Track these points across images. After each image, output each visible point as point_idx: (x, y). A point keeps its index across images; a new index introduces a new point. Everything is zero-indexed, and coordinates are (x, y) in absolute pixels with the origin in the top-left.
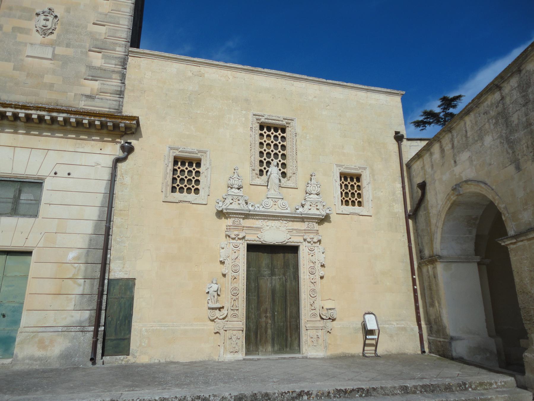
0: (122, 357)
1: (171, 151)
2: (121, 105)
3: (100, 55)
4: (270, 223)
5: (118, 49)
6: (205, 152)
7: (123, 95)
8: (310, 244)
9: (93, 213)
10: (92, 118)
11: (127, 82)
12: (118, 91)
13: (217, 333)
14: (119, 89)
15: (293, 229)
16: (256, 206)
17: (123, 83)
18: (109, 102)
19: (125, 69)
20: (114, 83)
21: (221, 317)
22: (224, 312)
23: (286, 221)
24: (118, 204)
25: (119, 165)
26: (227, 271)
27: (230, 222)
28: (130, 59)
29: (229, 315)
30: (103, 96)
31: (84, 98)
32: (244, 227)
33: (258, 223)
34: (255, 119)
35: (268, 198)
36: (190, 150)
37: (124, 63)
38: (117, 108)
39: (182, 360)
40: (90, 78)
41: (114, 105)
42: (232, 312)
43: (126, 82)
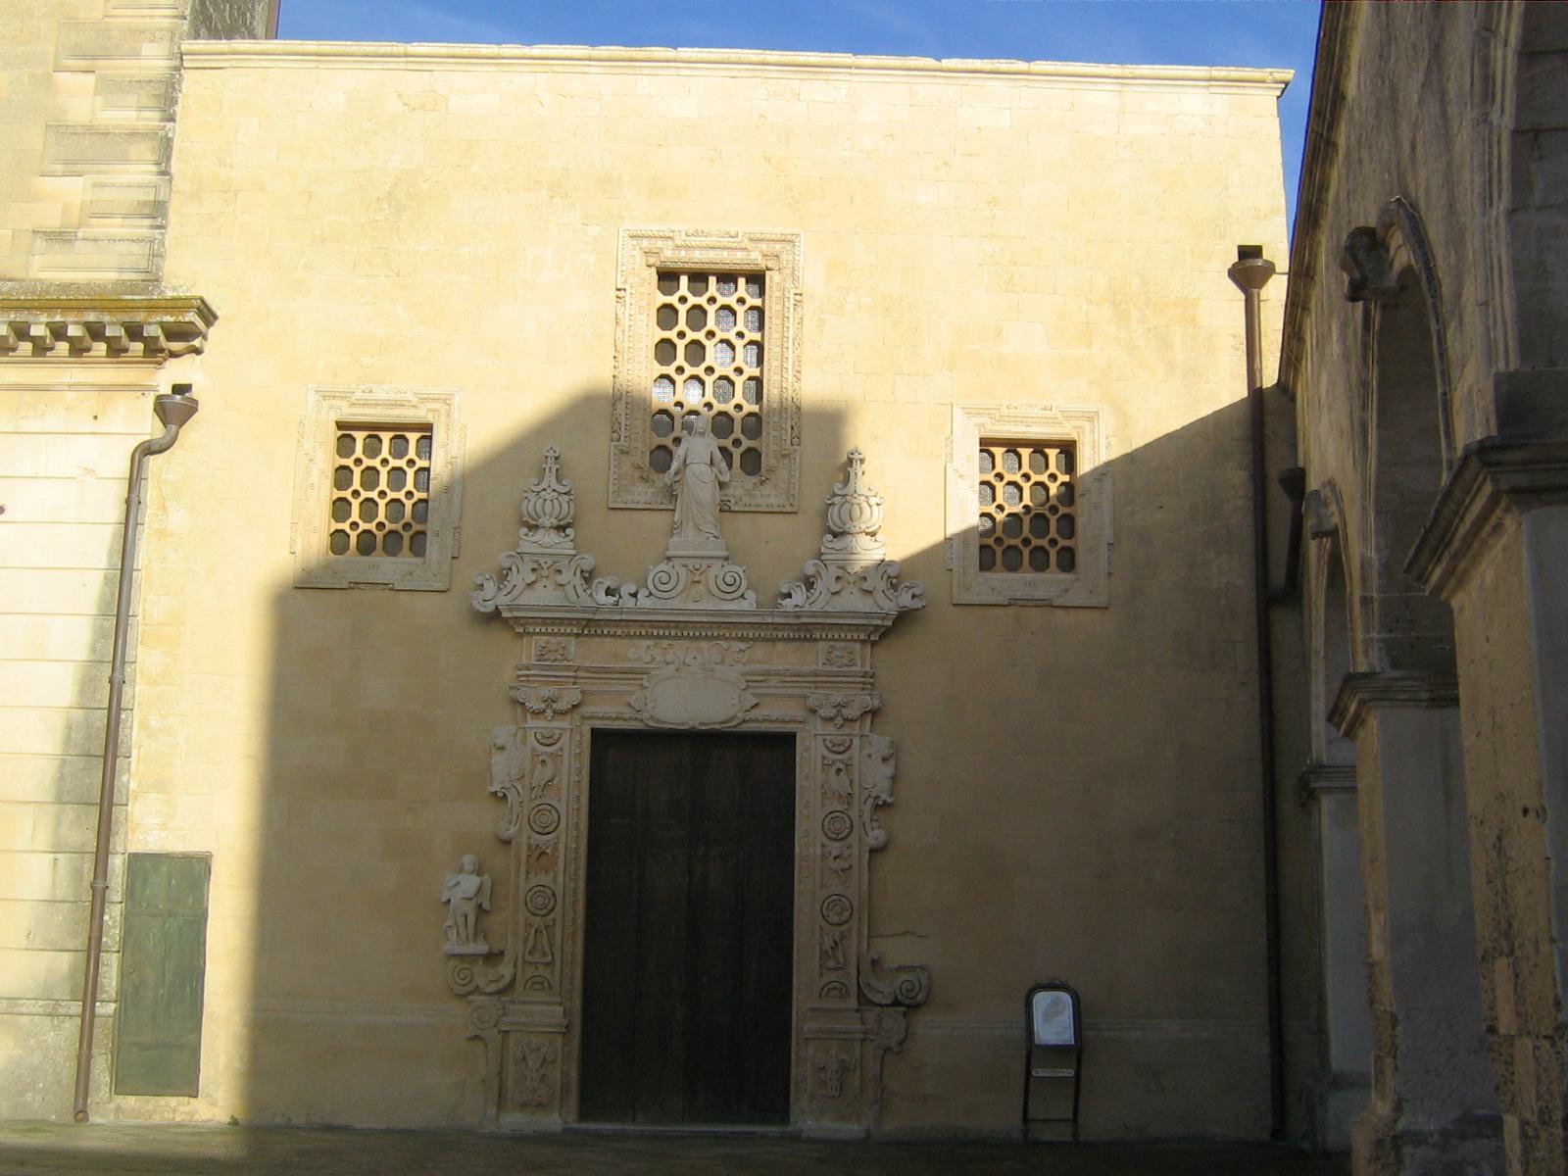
0: (173, 1101)
1: (326, 404)
2: (156, 255)
3: (91, 79)
4: (680, 651)
5: (148, 49)
6: (446, 401)
7: (165, 216)
8: (831, 729)
9: (75, 637)
10: (58, 318)
11: (175, 167)
12: (145, 203)
13: (476, 1037)
14: (151, 198)
15: (768, 673)
16: (625, 591)
17: (165, 173)
18: (120, 247)
19: (173, 120)
20: (137, 174)
21: (491, 988)
22: (506, 970)
23: (742, 639)
24: (147, 605)
25: (154, 462)
26: (513, 830)
27: (527, 651)
28: (189, 79)
29: (519, 983)
30: (98, 227)
31: (40, 243)
32: (578, 669)
33: (638, 652)
34: (637, 252)
35: (669, 559)
36: (392, 396)
37: (167, 96)
38: (143, 265)
39: (359, 1123)
40: (59, 168)
41: (134, 255)
42: (530, 972)
43: (174, 168)
